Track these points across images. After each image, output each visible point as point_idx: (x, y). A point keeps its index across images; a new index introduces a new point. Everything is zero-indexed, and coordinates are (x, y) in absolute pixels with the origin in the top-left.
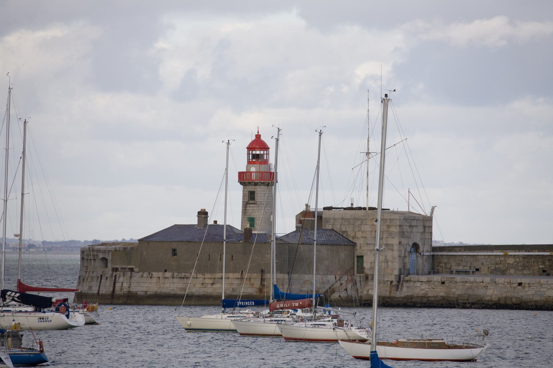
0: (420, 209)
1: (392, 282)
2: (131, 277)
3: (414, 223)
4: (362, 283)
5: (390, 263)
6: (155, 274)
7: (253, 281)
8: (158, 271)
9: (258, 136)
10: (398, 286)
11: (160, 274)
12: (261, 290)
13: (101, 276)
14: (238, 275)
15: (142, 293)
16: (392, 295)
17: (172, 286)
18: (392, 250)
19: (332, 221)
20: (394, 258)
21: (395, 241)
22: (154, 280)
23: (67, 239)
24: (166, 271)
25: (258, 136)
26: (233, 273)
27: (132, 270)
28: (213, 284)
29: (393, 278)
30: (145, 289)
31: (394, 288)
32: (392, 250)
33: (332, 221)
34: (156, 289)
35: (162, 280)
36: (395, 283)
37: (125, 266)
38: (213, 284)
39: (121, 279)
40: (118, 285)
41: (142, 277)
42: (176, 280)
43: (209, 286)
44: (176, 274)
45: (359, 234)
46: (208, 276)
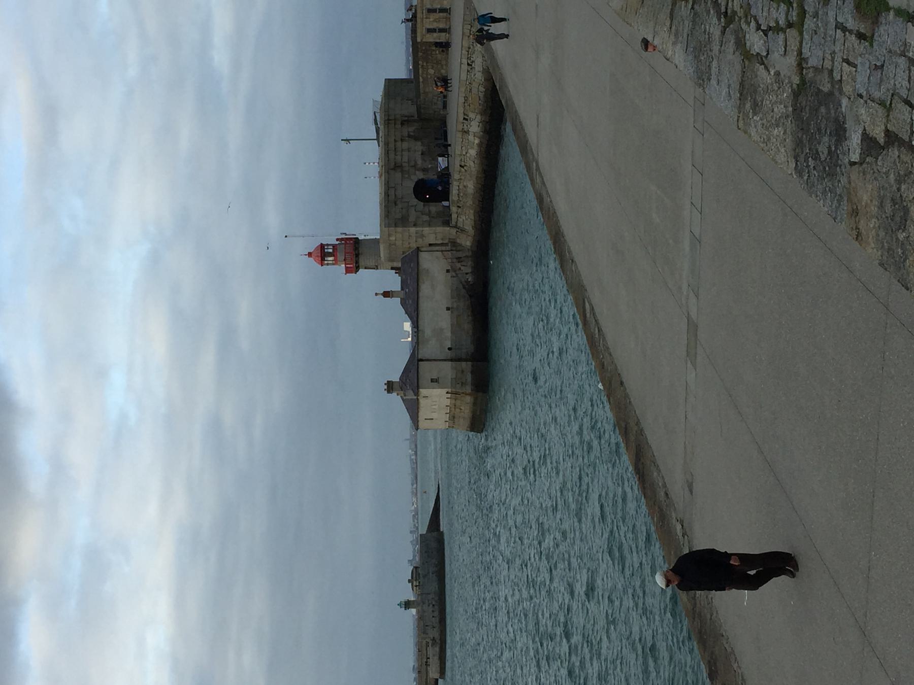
0: (378, 93)
3: (392, 197)
4: (459, 248)
9: (310, 254)
21: (413, 230)
25: (310, 254)
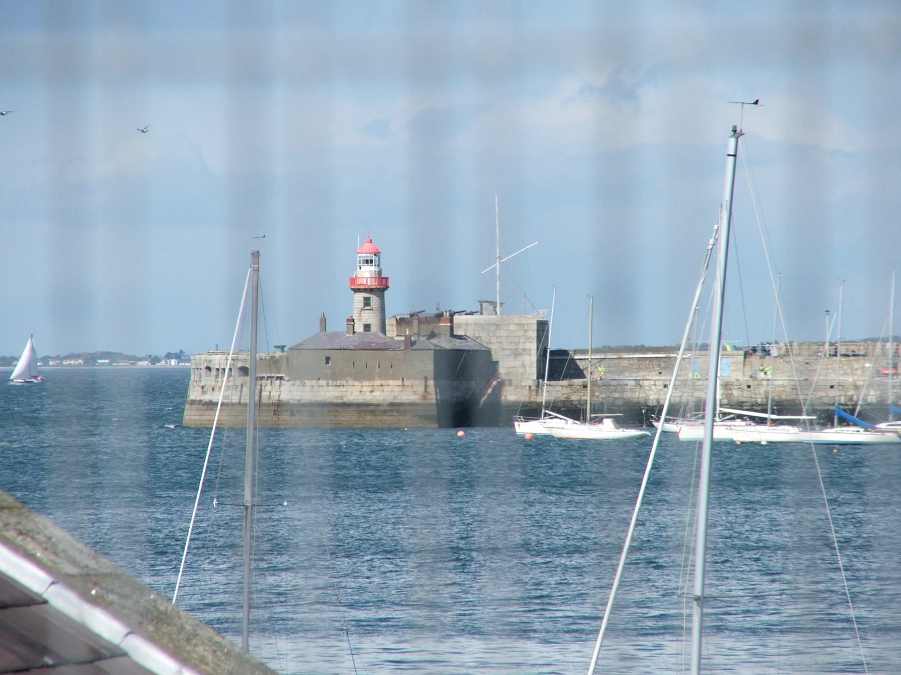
1: (530, 387)
2: (280, 386)
5: (527, 368)
6: (308, 382)
7: (415, 388)
8: (311, 379)
10: (537, 391)
11: (314, 382)
12: (424, 397)
13: (242, 385)
14: (399, 382)
15: (296, 402)
16: (532, 400)
17: (327, 393)
18: (530, 355)
19: (464, 326)
20: (531, 363)
22: (307, 388)
23: (92, 352)
24: (319, 379)
26: (393, 379)
27: (281, 378)
28: (371, 392)
29: (530, 383)
30: (297, 398)
31: (534, 393)
32: (530, 355)
33: (464, 326)
34: (310, 398)
35: (316, 389)
36: (533, 388)
37: (273, 375)
38: (371, 392)
39: (268, 388)
40: (265, 394)
41: (294, 385)
42: (331, 388)
43: (368, 394)
44: (330, 382)
45: (494, 340)
46: (366, 383)
